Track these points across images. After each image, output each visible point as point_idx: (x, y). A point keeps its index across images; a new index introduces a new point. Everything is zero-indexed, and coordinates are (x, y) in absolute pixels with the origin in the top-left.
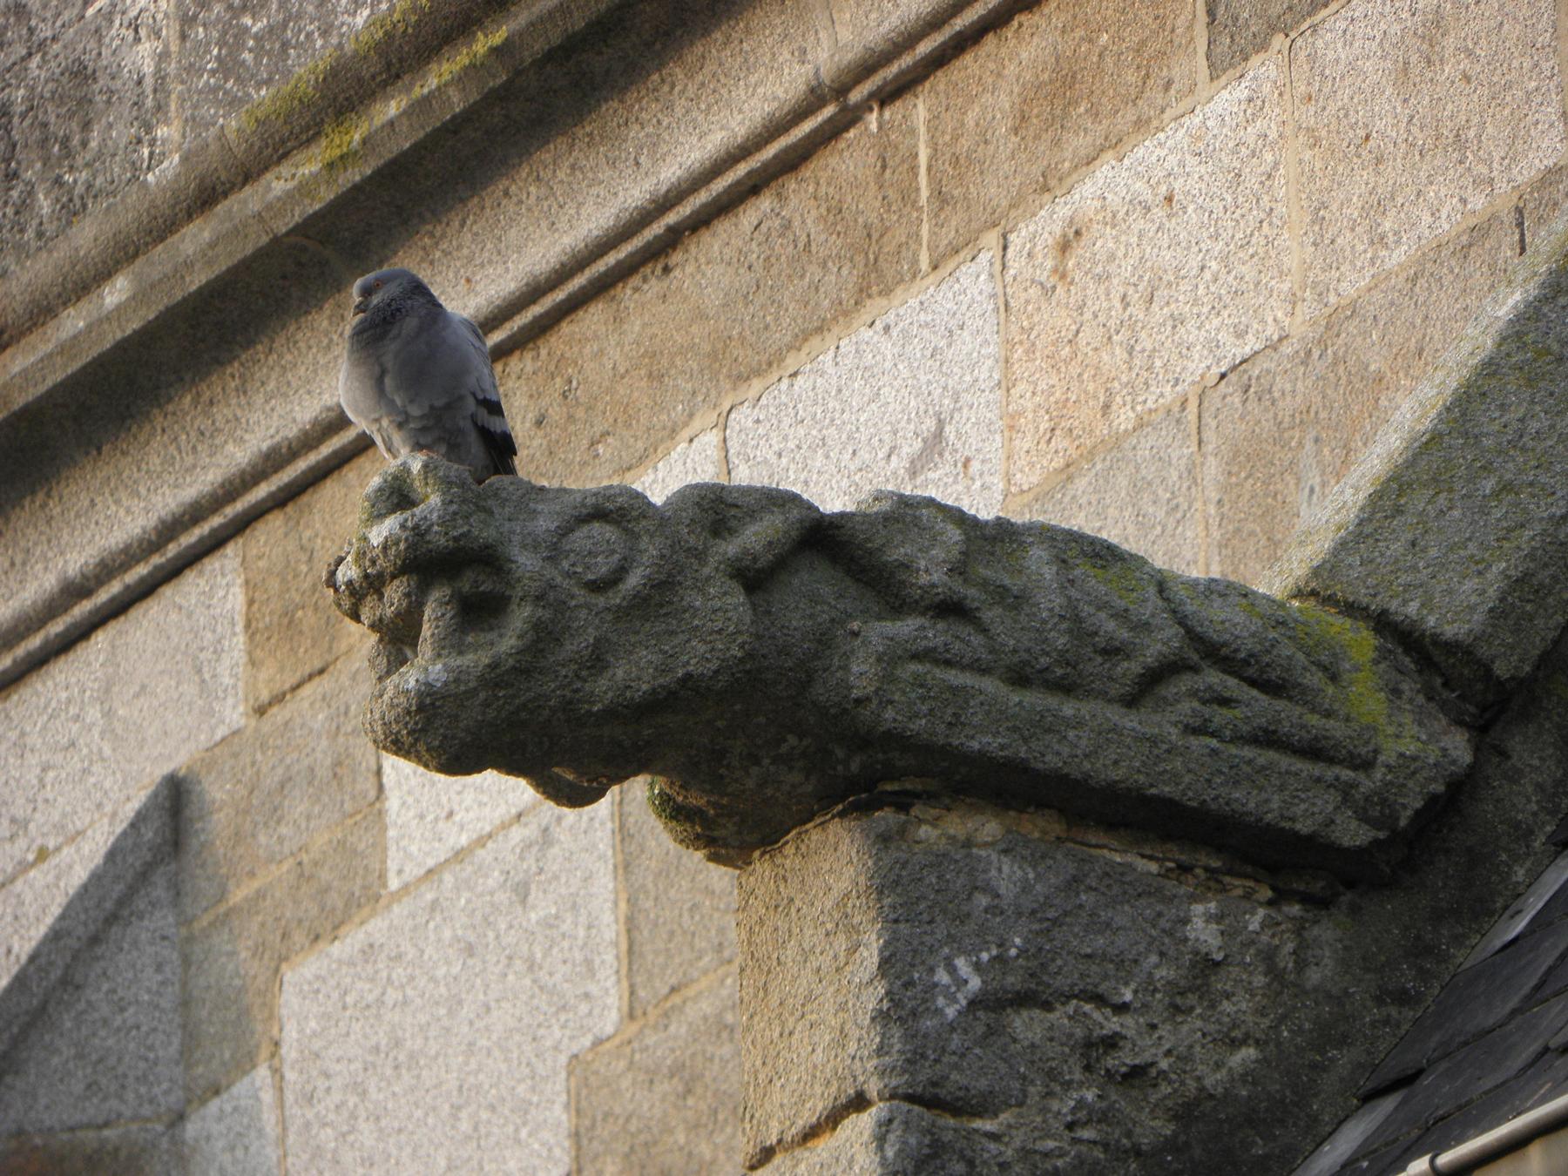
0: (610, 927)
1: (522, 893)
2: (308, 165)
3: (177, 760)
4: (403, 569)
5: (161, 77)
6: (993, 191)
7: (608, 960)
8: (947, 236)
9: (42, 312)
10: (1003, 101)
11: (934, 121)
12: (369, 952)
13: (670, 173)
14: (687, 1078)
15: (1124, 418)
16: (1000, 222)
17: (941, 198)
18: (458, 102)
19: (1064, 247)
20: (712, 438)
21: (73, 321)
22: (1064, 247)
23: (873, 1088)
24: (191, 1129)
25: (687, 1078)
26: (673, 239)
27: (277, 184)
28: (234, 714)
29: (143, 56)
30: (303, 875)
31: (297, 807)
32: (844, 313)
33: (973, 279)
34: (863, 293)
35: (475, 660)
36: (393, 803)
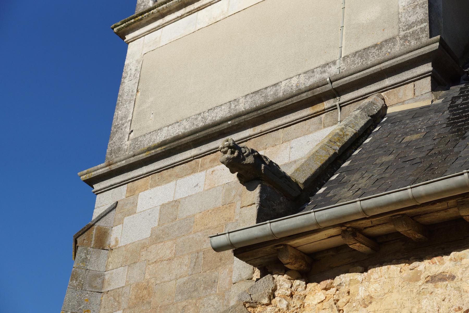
0: (158, 218)
1: (149, 214)
2: (144, 155)
3: (117, 200)
4: (227, 147)
5: (127, 149)
6: (206, 166)
7: (157, 221)
8: (202, 169)
9: (116, 162)
10: (209, 160)
11: (202, 161)
12: (133, 217)
13: (176, 161)
14: (163, 231)
15: (216, 185)
16: (207, 169)
17: (201, 166)
18: (159, 152)
19: (213, 172)
20: (175, 182)
21: (119, 164)
22: (213, 172)
23: (256, 202)
24: (113, 228)
25: (163, 231)
26: (175, 166)
27: (141, 155)
28: (124, 197)
29: (126, 147)
30: (128, 210)
31: (129, 205)
32: (190, 174)
33: (203, 173)
34: (192, 173)
35: (232, 156)
36: (138, 206)
